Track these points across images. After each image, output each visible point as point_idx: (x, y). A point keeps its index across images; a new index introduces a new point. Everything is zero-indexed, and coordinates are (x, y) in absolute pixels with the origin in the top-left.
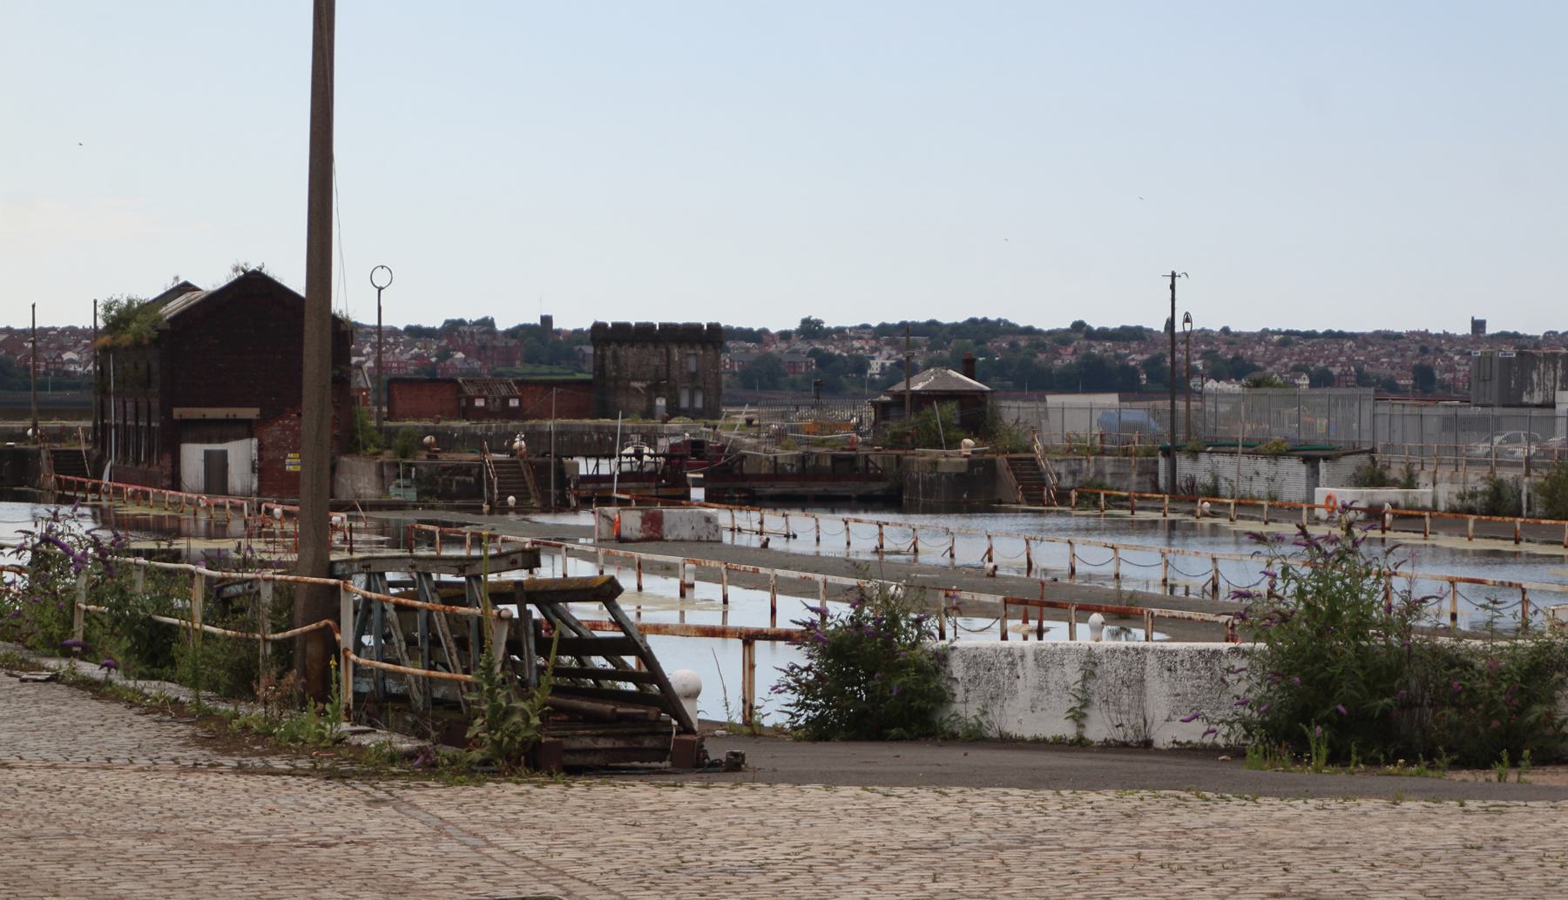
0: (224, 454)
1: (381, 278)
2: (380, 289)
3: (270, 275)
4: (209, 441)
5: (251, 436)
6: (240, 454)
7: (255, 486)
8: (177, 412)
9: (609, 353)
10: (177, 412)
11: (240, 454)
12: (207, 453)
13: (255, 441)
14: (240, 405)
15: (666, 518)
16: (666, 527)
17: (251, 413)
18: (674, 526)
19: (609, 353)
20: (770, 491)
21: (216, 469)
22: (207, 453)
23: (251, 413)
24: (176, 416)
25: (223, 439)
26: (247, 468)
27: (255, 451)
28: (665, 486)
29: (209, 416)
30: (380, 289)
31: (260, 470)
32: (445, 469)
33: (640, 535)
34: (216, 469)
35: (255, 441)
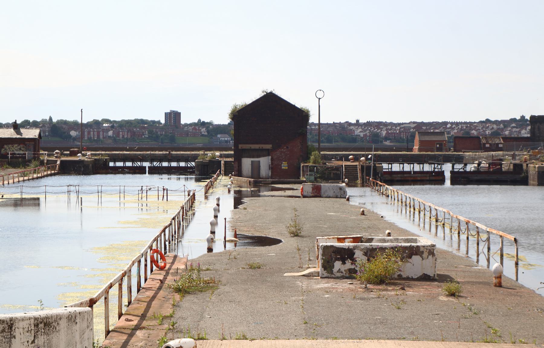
0: (259, 162)
1: (320, 95)
2: (319, 99)
3: (276, 94)
4: (253, 157)
5: (268, 155)
6: (265, 162)
7: (270, 174)
8: (240, 146)
9: (536, 127)
10: (240, 146)
11: (265, 162)
12: (252, 162)
13: (270, 157)
14: (264, 144)
15: (322, 188)
16: (322, 191)
17: (269, 146)
18: (326, 191)
19: (536, 127)
20: (476, 178)
21: (256, 167)
22: (252, 162)
23: (269, 146)
24: (240, 148)
25: (258, 156)
26: (267, 168)
27: (270, 161)
28: (434, 176)
29: (264, 148)
30: (319, 99)
31: (272, 168)
32: (328, 168)
33: (311, 195)
34: (256, 167)
35: (270, 157)
